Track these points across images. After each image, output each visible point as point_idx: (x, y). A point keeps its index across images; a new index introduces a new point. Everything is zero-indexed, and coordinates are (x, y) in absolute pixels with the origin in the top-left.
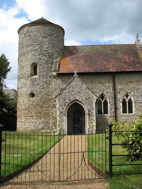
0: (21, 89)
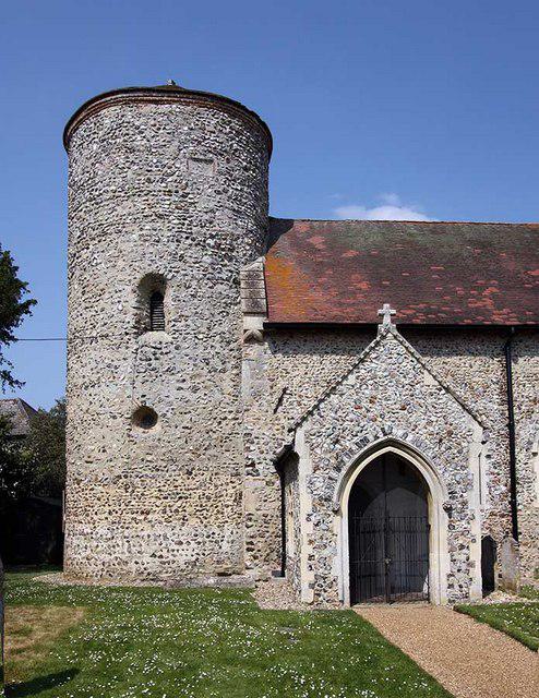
0: (91, 390)
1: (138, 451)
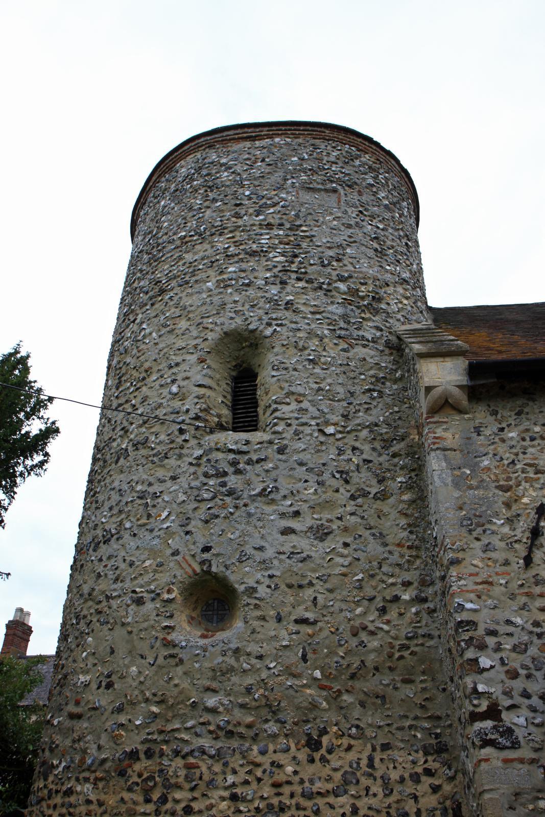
0: (104, 550)
1: (185, 684)
